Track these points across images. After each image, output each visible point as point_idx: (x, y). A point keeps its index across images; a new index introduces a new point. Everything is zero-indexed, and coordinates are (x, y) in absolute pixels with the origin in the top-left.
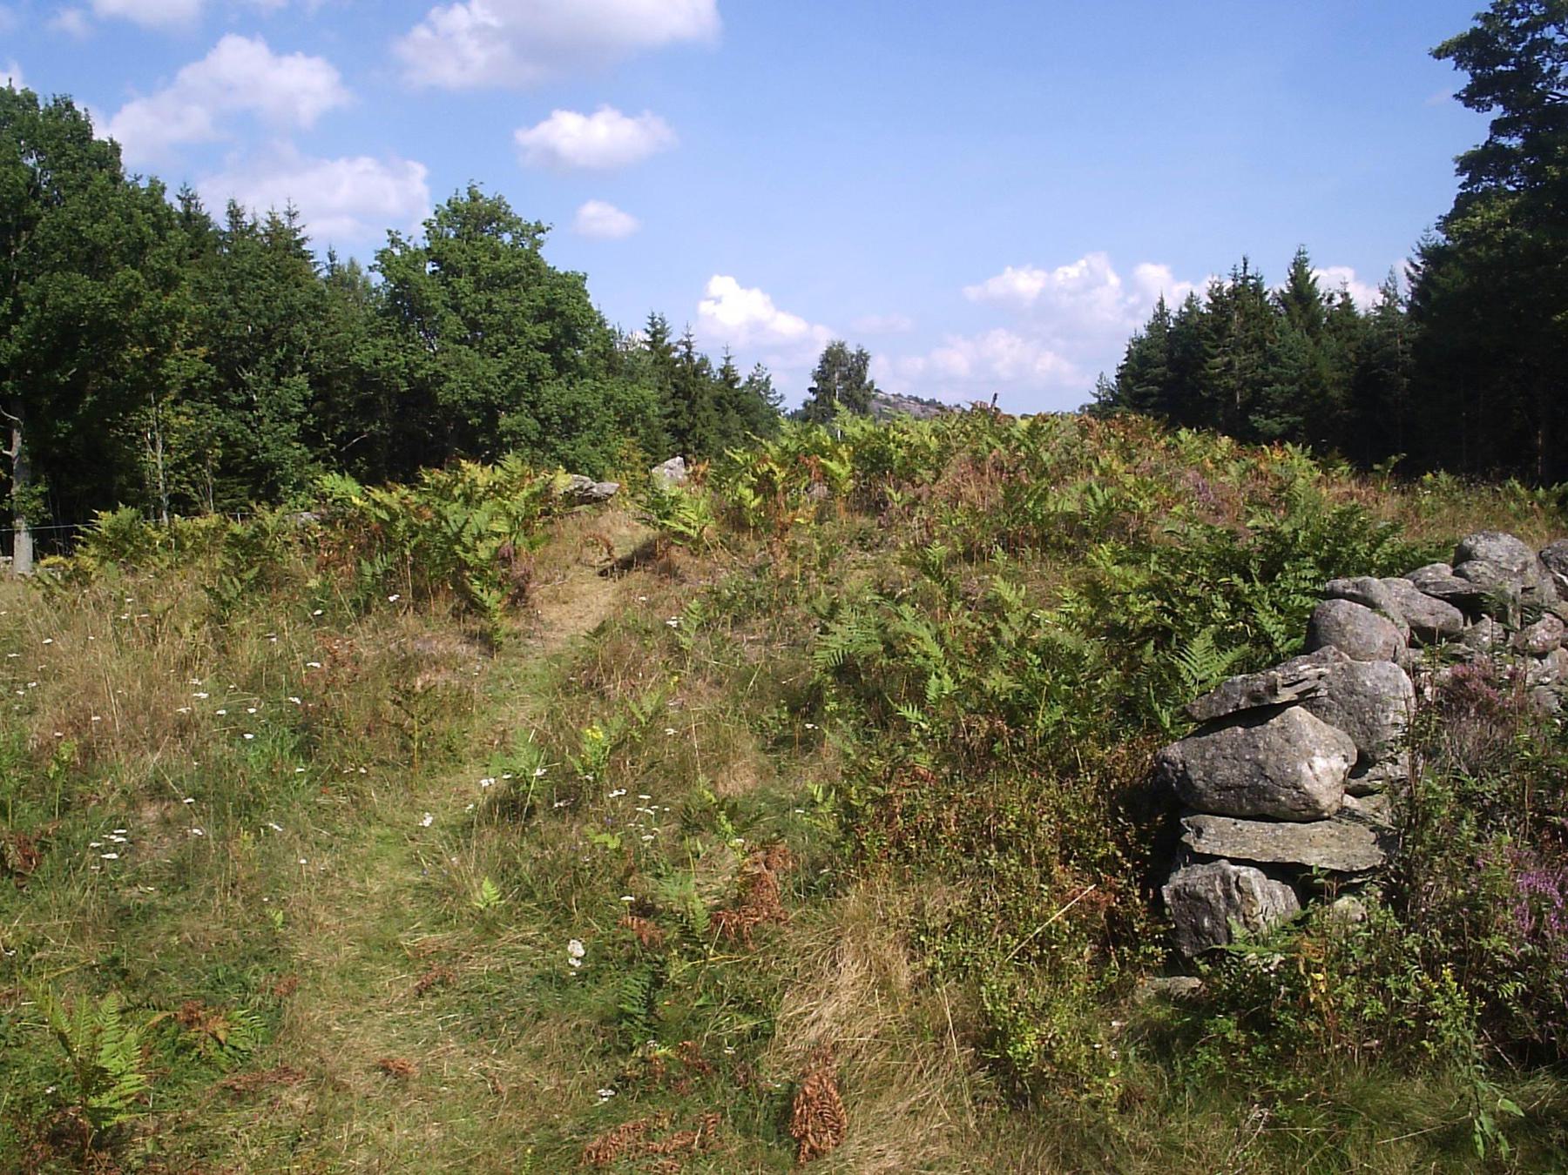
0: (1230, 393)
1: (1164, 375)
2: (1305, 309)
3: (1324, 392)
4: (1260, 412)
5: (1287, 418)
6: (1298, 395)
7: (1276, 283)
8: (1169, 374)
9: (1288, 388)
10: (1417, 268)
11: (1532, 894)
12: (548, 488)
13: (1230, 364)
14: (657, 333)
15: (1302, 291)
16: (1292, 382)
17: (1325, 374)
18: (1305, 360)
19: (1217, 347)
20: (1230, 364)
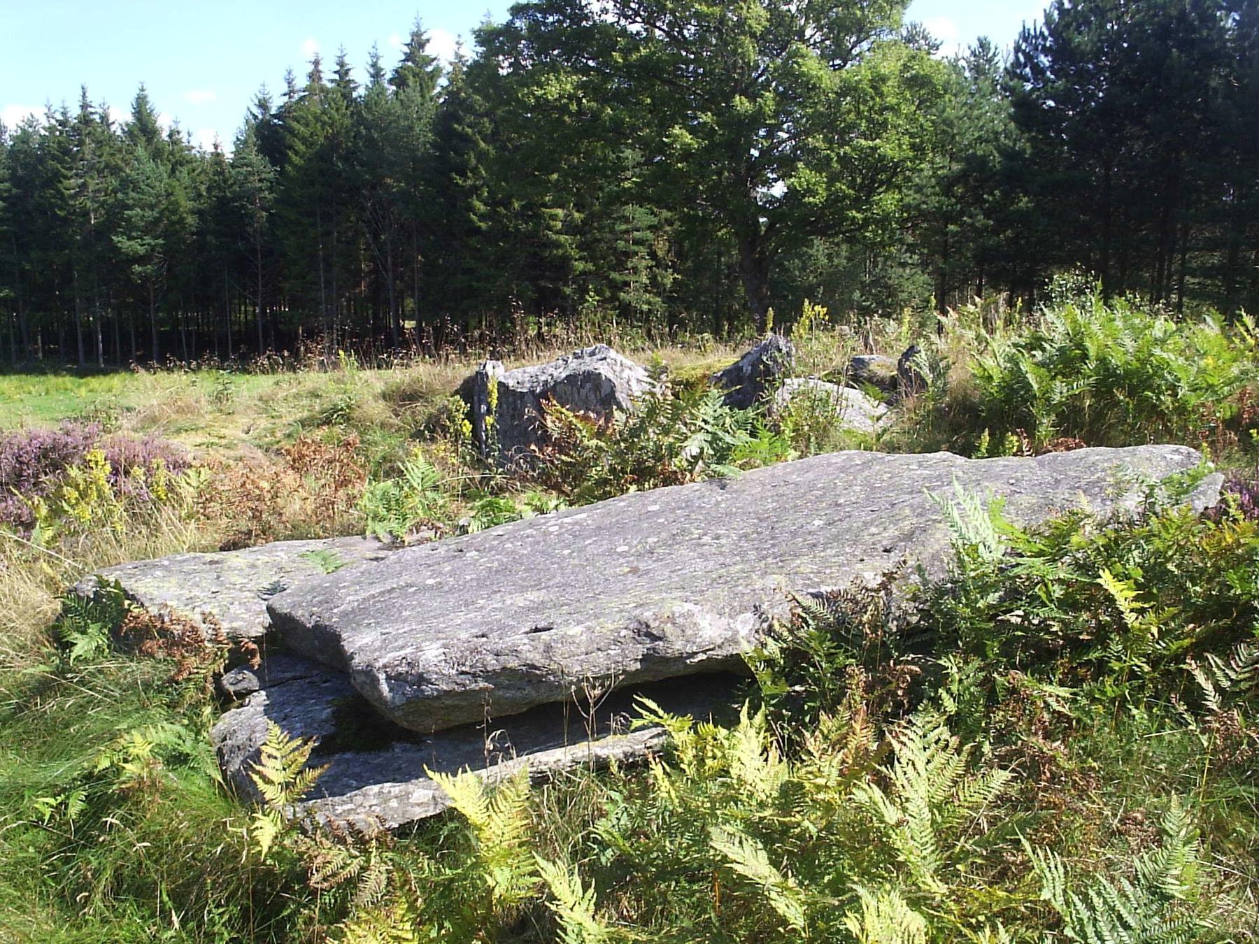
0: (86, 214)
1: (9, 191)
2: (149, 141)
3: (182, 219)
4: (123, 234)
5: (148, 240)
6: (157, 221)
7: (121, 116)
8: (14, 191)
9: (148, 213)
10: (255, 117)
11: (1154, 664)
12: (481, 377)
13: (84, 185)
14: (141, 110)
15: (143, 125)
16: (152, 207)
17: (183, 203)
18: (161, 187)
19: (70, 169)
20: (84, 185)
